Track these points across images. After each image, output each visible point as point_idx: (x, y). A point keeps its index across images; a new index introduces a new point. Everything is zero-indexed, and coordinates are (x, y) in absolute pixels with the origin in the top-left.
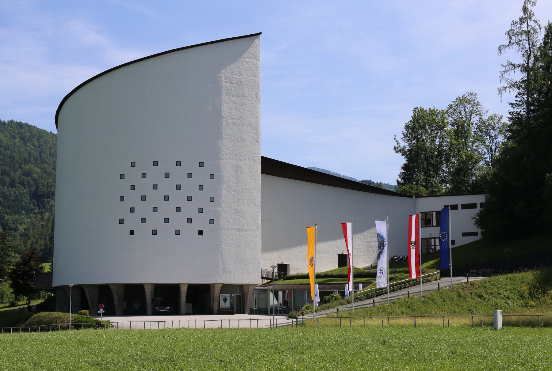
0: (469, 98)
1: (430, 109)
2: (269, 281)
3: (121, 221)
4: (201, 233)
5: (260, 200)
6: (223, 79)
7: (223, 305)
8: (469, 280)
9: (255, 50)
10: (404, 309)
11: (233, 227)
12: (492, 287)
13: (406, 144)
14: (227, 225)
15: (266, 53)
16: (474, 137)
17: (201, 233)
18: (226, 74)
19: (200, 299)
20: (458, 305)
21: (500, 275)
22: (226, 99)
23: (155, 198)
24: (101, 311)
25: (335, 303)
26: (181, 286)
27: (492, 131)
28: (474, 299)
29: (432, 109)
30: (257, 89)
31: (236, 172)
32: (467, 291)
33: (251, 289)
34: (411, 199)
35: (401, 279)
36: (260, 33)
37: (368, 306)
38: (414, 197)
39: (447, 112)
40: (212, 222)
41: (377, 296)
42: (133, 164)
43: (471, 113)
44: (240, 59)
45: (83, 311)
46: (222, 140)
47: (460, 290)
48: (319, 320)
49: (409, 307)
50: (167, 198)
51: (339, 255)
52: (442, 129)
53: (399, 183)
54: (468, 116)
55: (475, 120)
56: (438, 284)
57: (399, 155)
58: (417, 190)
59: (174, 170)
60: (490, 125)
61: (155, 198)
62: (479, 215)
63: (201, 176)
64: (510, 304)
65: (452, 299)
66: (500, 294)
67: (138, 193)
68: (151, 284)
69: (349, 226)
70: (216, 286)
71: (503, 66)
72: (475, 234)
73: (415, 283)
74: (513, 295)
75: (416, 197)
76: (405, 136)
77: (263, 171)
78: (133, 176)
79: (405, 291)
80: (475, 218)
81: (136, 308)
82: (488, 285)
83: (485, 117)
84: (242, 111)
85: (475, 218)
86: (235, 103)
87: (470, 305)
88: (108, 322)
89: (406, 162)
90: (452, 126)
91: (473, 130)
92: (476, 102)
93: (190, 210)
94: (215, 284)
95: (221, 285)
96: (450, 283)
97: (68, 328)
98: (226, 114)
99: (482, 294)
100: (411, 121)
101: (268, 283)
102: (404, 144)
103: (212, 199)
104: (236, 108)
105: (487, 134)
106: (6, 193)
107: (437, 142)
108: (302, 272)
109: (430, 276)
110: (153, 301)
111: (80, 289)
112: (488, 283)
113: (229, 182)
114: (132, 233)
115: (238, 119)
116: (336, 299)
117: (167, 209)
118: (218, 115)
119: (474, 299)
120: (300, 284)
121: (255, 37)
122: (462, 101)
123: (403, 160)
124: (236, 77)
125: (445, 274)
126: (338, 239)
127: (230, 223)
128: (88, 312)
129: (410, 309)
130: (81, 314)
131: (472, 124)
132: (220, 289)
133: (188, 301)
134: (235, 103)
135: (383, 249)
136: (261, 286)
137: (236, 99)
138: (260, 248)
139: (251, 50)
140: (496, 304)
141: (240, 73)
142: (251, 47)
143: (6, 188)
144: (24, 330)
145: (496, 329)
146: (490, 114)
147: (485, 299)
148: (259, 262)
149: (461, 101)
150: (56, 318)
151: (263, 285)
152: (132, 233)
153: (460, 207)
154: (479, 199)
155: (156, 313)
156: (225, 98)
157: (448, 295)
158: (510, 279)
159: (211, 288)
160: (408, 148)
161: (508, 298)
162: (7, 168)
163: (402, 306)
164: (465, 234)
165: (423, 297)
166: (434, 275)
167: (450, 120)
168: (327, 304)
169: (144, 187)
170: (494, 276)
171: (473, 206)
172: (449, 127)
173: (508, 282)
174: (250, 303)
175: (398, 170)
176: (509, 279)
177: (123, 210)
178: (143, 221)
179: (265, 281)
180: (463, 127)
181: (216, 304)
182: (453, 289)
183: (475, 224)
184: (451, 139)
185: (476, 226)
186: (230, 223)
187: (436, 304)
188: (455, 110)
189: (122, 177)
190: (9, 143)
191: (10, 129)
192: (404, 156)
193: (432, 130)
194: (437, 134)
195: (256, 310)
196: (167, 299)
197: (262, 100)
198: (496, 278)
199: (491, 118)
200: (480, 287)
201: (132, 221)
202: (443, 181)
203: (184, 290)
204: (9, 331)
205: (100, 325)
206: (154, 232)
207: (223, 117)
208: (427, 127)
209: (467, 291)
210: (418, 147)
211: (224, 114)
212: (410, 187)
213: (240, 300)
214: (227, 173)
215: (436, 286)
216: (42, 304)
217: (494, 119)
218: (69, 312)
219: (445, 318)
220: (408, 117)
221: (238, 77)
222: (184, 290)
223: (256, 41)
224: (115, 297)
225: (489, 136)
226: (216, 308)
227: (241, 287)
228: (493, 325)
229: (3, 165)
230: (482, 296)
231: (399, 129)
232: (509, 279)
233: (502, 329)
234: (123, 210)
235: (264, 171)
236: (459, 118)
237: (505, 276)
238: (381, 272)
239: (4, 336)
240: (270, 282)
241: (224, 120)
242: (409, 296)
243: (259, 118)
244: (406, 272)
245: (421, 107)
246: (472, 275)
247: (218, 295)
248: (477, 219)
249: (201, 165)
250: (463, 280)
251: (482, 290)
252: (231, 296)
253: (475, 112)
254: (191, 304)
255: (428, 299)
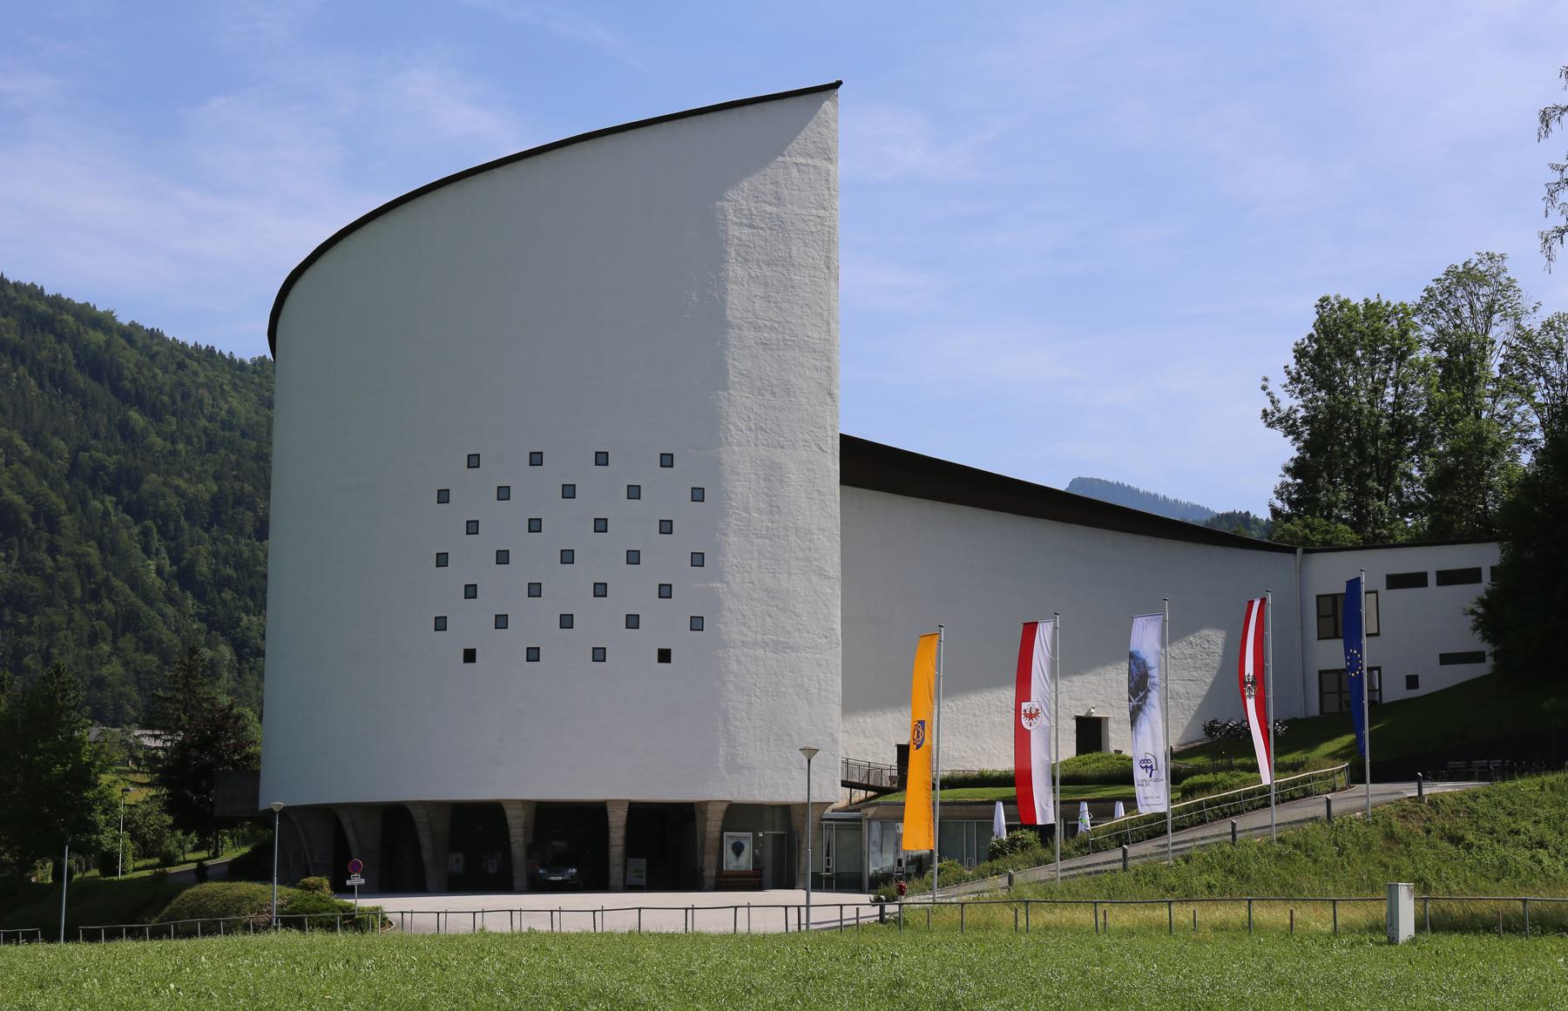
0: (1481, 268)
1: (1367, 301)
2: (870, 793)
3: (441, 624)
4: (664, 656)
5: (837, 560)
6: (731, 217)
7: (732, 863)
8: (1426, 791)
9: (824, 131)
10: (1216, 878)
11: (759, 637)
12: (1492, 812)
13: (1297, 402)
14: (743, 634)
15: (865, 141)
16: (1497, 380)
17: (664, 656)
18: (739, 201)
19: (667, 844)
20: (1386, 866)
21: (1521, 776)
22: (740, 272)
23: (535, 557)
24: (356, 880)
25: (1020, 857)
26: (609, 809)
27: (1552, 364)
28: (1434, 847)
29: (1373, 300)
30: (827, 243)
31: (767, 480)
32: (1415, 825)
33: (812, 819)
34: (1290, 556)
35: (1225, 789)
36: (838, 84)
37: (1107, 867)
38: (1299, 551)
39: (1419, 309)
40: (697, 624)
41: (1149, 837)
42: (473, 461)
43: (1490, 310)
44: (780, 159)
45: (312, 880)
46: (726, 388)
47: (1394, 819)
48: (742, 913)
49: (1231, 871)
50: (633, 557)
51: (1079, 720)
52: (1402, 357)
53: (1276, 512)
54: (1480, 320)
55: (1500, 331)
56: (1328, 801)
57: (1278, 433)
58: (1327, 532)
59: (588, 477)
60: (1548, 345)
61: (535, 557)
62: (1482, 602)
63: (665, 493)
64: (1546, 861)
65: (1368, 847)
66: (1517, 833)
67: (486, 543)
68: (526, 803)
69: (1044, 633)
70: (710, 807)
71: (1554, 167)
72: (1477, 657)
73: (1260, 799)
74: (1556, 834)
75: (1306, 552)
76: (1296, 379)
77: (848, 478)
78: (473, 496)
79: (1225, 827)
80: (1472, 612)
81: (492, 870)
82: (1481, 806)
83: (1533, 323)
84: (785, 305)
85: (1472, 612)
86: (766, 284)
87: (1421, 866)
88: (376, 911)
89: (1296, 455)
90: (1434, 349)
91: (1495, 364)
92: (1504, 282)
93: (632, 590)
94: (707, 803)
95: (724, 806)
96: (1364, 801)
97: (267, 926)
98: (737, 314)
99: (1461, 833)
100: (1311, 336)
101: (867, 799)
102: (1289, 402)
103: (698, 560)
104: (767, 298)
105: (1539, 372)
106: (246, 555)
107: (1389, 395)
108: (969, 767)
109: (1314, 778)
110: (530, 850)
111: (329, 815)
112: (1482, 800)
113: (746, 510)
114: (470, 656)
115: (773, 329)
116: (1025, 846)
117: (567, 589)
118: (714, 319)
119: (1434, 847)
120: (955, 803)
121: (822, 95)
122: (1465, 277)
123: (1286, 450)
124: (768, 208)
125: (1357, 777)
126: (1076, 673)
127: (749, 627)
128: (326, 882)
129: (1236, 877)
130: (306, 887)
131: (1493, 342)
132: (721, 816)
133: (631, 850)
134: (766, 284)
135: (1145, 697)
136: (845, 809)
137: (767, 271)
138: (838, 700)
139: (810, 132)
140: (1504, 862)
141: (778, 198)
142: (812, 124)
143: (243, 541)
144: (157, 934)
145: (1393, 940)
146: (1545, 314)
147: (1469, 847)
148: (834, 741)
149: (1459, 278)
150: (240, 899)
151: (852, 807)
152: (470, 656)
153: (1432, 579)
154: (1485, 556)
155: (539, 886)
156: (735, 270)
157: (1356, 835)
158: (1552, 789)
159: (698, 816)
160: (1302, 413)
161: (1542, 844)
162: (248, 488)
163: (1211, 869)
164: (1446, 659)
165: (1280, 840)
166: (1327, 776)
167: (1428, 332)
168: (995, 862)
169: (503, 524)
170: (1503, 780)
171: (1471, 576)
172: (1423, 353)
173: (1544, 797)
174: (810, 860)
175: (1275, 477)
176: (1547, 788)
177: (444, 591)
178: (501, 622)
179: (860, 795)
180: (1466, 348)
181: (709, 860)
182: (1372, 818)
183: (1475, 629)
184: (1428, 386)
185: (1478, 635)
186: (749, 627)
187: (1315, 861)
188: (1441, 304)
189: (443, 496)
190: (256, 418)
191: (257, 380)
192: (1291, 437)
193: (1373, 362)
194: (1387, 371)
195: (829, 879)
196: (573, 845)
197: (844, 274)
198: (1509, 784)
199: (1549, 325)
200: (1456, 812)
201: (471, 624)
202: (1406, 509)
203: (617, 821)
204: (113, 935)
205: (356, 922)
206: (533, 655)
207: (729, 325)
208: (1359, 353)
209: (1415, 825)
210: (1334, 412)
211: (734, 313)
212: (1306, 526)
213: (779, 846)
214: (742, 486)
215: (1321, 811)
216: (244, 857)
217: (1560, 329)
218: (270, 880)
219: (1100, 909)
220: (1304, 326)
221: (775, 210)
222: (617, 821)
223: (827, 105)
224: (425, 841)
225: (1545, 376)
226: (710, 873)
227: (786, 809)
228: (1386, 929)
229: (236, 478)
230: (1462, 839)
231: (1277, 359)
232: (1547, 788)
233: (1413, 941)
234: (444, 591)
235: (848, 477)
236: (1456, 326)
237: (1538, 780)
238: (1148, 767)
239: (17, 953)
240: (874, 797)
241: (733, 333)
242: (1234, 838)
243: (833, 326)
244: (1244, 768)
245: (1337, 297)
246: (1437, 778)
247: (717, 835)
248: (1479, 615)
249: (667, 460)
250: (1409, 790)
251: (1462, 821)
252: (755, 837)
253: (1502, 308)
254: (643, 861)
255: (1294, 848)
